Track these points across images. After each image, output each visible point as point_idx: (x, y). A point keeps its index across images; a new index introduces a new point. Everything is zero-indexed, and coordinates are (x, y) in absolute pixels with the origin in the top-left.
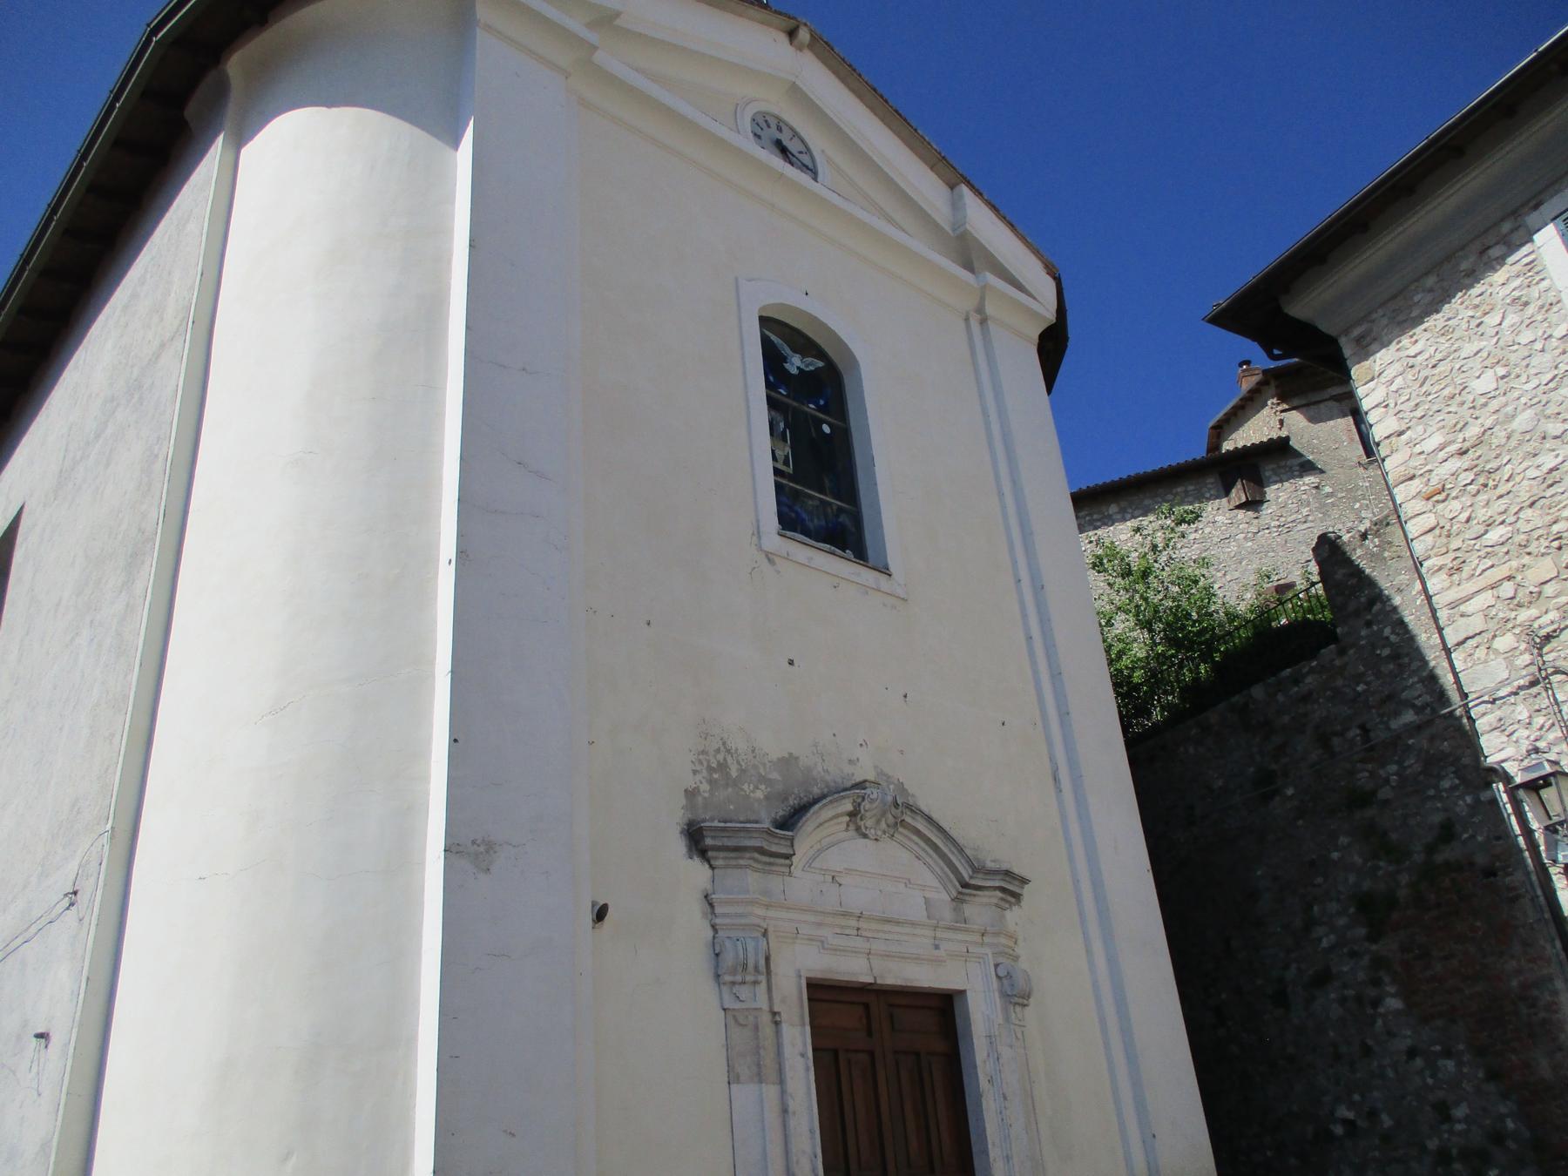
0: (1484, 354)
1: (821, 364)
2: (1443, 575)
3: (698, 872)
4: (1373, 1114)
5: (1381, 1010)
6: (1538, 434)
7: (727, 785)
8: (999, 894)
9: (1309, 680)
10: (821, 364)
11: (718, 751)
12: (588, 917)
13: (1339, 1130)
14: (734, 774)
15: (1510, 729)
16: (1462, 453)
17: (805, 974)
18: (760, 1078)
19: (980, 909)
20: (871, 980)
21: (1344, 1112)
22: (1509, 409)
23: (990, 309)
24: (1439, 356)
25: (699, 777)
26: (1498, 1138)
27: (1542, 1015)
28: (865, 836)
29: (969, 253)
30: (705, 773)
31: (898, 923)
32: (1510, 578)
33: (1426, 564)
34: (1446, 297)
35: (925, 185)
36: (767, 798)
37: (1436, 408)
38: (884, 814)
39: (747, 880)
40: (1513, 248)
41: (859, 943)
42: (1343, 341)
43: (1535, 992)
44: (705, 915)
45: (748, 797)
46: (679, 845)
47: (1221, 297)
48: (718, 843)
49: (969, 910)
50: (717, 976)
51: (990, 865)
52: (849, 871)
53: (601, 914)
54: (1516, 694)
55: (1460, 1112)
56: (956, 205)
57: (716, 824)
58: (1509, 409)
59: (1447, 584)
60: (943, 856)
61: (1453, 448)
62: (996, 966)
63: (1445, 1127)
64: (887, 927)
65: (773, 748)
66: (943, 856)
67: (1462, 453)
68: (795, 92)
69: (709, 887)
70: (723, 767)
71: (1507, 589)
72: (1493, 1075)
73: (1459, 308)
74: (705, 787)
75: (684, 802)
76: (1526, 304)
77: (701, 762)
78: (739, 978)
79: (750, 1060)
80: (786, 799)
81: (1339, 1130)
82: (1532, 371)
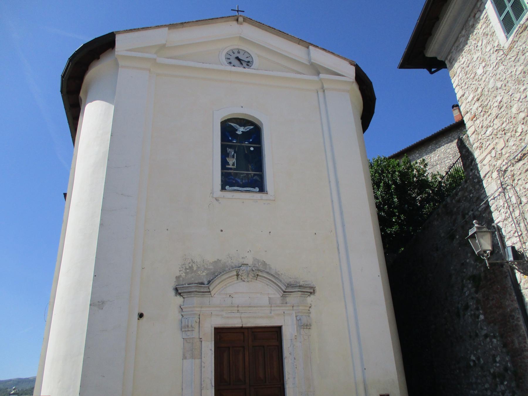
0: (479, 58)
1: (252, 127)
2: (478, 150)
3: (179, 300)
4: (478, 359)
5: (479, 320)
6: (495, 88)
7: (192, 273)
8: (300, 293)
9: (459, 194)
10: (252, 127)
11: (190, 263)
12: (136, 316)
13: (472, 364)
14: (195, 269)
15: (499, 209)
16: (478, 100)
17: (213, 326)
18: (193, 357)
19: (293, 299)
20: (241, 326)
21: (473, 358)
22: (487, 80)
23: (325, 86)
24: (469, 62)
25: (181, 272)
26: (506, 369)
27: (516, 322)
28: (244, 281)
29: (317, 69)
30: (184, 270)
31: (261, 307)
32: (494, 148)
33: (474, 146)
34: (468, 39)
35: (297, 51)
36: (207, 274)
37: (470, 83)
38: (248, 274)
39: (195, 300)
40: (481, 12)
41: (238, 315)
42: (446, 62)
43: (513, 314)
44: (179, 312)
45: (200, 275)
46: (173, 293)
47: (399, 60)
48: (182, 291)
49: (288, 299)
50: (181, 329)
51: (302, 283)
52: (236, 293)
53: (141, 316)
54: (499, 195)
55: (498, 359)
56: (309, 54)
57: (187, 285)
58: (487, 80)
59: (479, 153)
60: (275, 283)
61: (475, 99)
62: (296, 316)
63: (494, 364)
64: (249, 309)
65: (210, 258)
66: (275, 283)
67: (478, 100)
68: (242, 39)
69: (182, 304)
70: (191, 268)
71: (493, 154)
72: (505, 345)
73: (471, 41)
74: (184, 274)
75: (175, 280)
76: (487, 35)
77: (183, 268)
78: (187, 330)
79: (191, 351)
80: (214, 274)
81: (472, 364)
82: (491, 62)
